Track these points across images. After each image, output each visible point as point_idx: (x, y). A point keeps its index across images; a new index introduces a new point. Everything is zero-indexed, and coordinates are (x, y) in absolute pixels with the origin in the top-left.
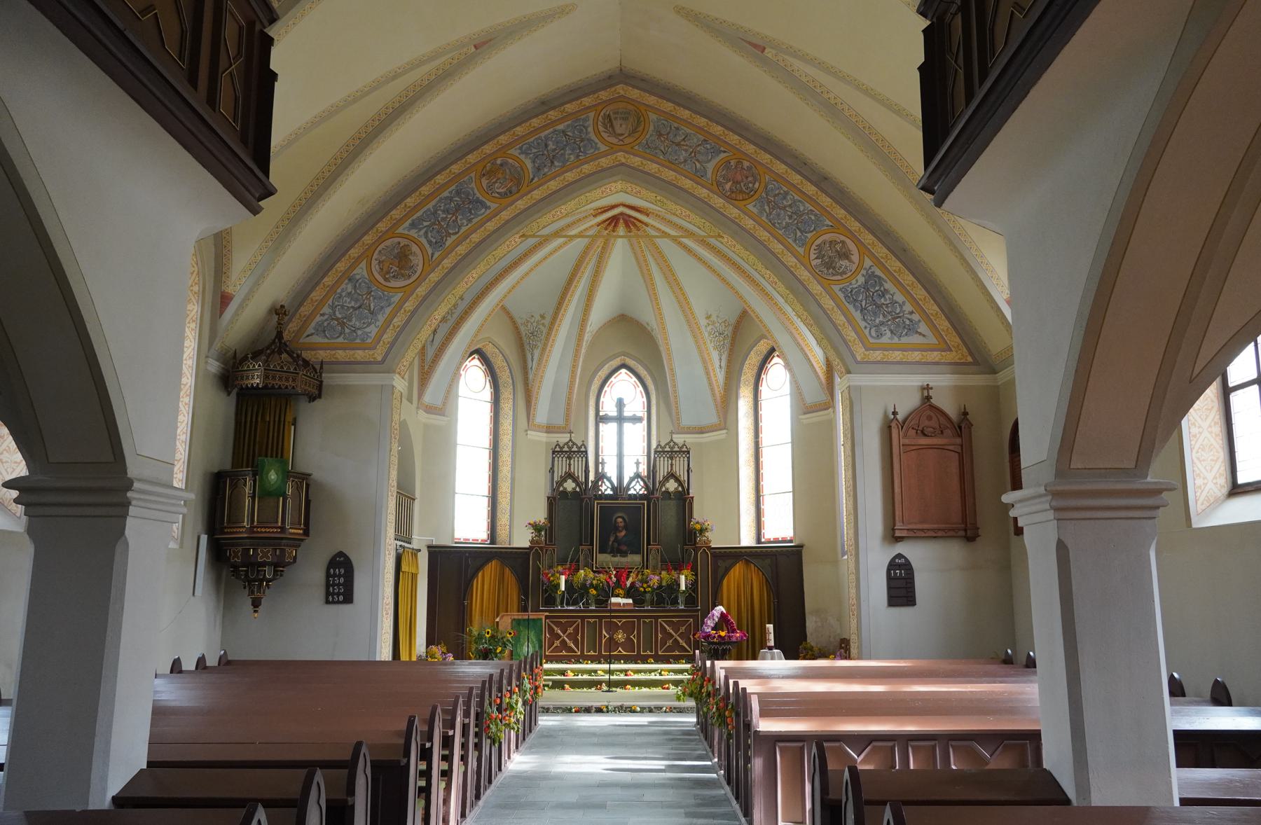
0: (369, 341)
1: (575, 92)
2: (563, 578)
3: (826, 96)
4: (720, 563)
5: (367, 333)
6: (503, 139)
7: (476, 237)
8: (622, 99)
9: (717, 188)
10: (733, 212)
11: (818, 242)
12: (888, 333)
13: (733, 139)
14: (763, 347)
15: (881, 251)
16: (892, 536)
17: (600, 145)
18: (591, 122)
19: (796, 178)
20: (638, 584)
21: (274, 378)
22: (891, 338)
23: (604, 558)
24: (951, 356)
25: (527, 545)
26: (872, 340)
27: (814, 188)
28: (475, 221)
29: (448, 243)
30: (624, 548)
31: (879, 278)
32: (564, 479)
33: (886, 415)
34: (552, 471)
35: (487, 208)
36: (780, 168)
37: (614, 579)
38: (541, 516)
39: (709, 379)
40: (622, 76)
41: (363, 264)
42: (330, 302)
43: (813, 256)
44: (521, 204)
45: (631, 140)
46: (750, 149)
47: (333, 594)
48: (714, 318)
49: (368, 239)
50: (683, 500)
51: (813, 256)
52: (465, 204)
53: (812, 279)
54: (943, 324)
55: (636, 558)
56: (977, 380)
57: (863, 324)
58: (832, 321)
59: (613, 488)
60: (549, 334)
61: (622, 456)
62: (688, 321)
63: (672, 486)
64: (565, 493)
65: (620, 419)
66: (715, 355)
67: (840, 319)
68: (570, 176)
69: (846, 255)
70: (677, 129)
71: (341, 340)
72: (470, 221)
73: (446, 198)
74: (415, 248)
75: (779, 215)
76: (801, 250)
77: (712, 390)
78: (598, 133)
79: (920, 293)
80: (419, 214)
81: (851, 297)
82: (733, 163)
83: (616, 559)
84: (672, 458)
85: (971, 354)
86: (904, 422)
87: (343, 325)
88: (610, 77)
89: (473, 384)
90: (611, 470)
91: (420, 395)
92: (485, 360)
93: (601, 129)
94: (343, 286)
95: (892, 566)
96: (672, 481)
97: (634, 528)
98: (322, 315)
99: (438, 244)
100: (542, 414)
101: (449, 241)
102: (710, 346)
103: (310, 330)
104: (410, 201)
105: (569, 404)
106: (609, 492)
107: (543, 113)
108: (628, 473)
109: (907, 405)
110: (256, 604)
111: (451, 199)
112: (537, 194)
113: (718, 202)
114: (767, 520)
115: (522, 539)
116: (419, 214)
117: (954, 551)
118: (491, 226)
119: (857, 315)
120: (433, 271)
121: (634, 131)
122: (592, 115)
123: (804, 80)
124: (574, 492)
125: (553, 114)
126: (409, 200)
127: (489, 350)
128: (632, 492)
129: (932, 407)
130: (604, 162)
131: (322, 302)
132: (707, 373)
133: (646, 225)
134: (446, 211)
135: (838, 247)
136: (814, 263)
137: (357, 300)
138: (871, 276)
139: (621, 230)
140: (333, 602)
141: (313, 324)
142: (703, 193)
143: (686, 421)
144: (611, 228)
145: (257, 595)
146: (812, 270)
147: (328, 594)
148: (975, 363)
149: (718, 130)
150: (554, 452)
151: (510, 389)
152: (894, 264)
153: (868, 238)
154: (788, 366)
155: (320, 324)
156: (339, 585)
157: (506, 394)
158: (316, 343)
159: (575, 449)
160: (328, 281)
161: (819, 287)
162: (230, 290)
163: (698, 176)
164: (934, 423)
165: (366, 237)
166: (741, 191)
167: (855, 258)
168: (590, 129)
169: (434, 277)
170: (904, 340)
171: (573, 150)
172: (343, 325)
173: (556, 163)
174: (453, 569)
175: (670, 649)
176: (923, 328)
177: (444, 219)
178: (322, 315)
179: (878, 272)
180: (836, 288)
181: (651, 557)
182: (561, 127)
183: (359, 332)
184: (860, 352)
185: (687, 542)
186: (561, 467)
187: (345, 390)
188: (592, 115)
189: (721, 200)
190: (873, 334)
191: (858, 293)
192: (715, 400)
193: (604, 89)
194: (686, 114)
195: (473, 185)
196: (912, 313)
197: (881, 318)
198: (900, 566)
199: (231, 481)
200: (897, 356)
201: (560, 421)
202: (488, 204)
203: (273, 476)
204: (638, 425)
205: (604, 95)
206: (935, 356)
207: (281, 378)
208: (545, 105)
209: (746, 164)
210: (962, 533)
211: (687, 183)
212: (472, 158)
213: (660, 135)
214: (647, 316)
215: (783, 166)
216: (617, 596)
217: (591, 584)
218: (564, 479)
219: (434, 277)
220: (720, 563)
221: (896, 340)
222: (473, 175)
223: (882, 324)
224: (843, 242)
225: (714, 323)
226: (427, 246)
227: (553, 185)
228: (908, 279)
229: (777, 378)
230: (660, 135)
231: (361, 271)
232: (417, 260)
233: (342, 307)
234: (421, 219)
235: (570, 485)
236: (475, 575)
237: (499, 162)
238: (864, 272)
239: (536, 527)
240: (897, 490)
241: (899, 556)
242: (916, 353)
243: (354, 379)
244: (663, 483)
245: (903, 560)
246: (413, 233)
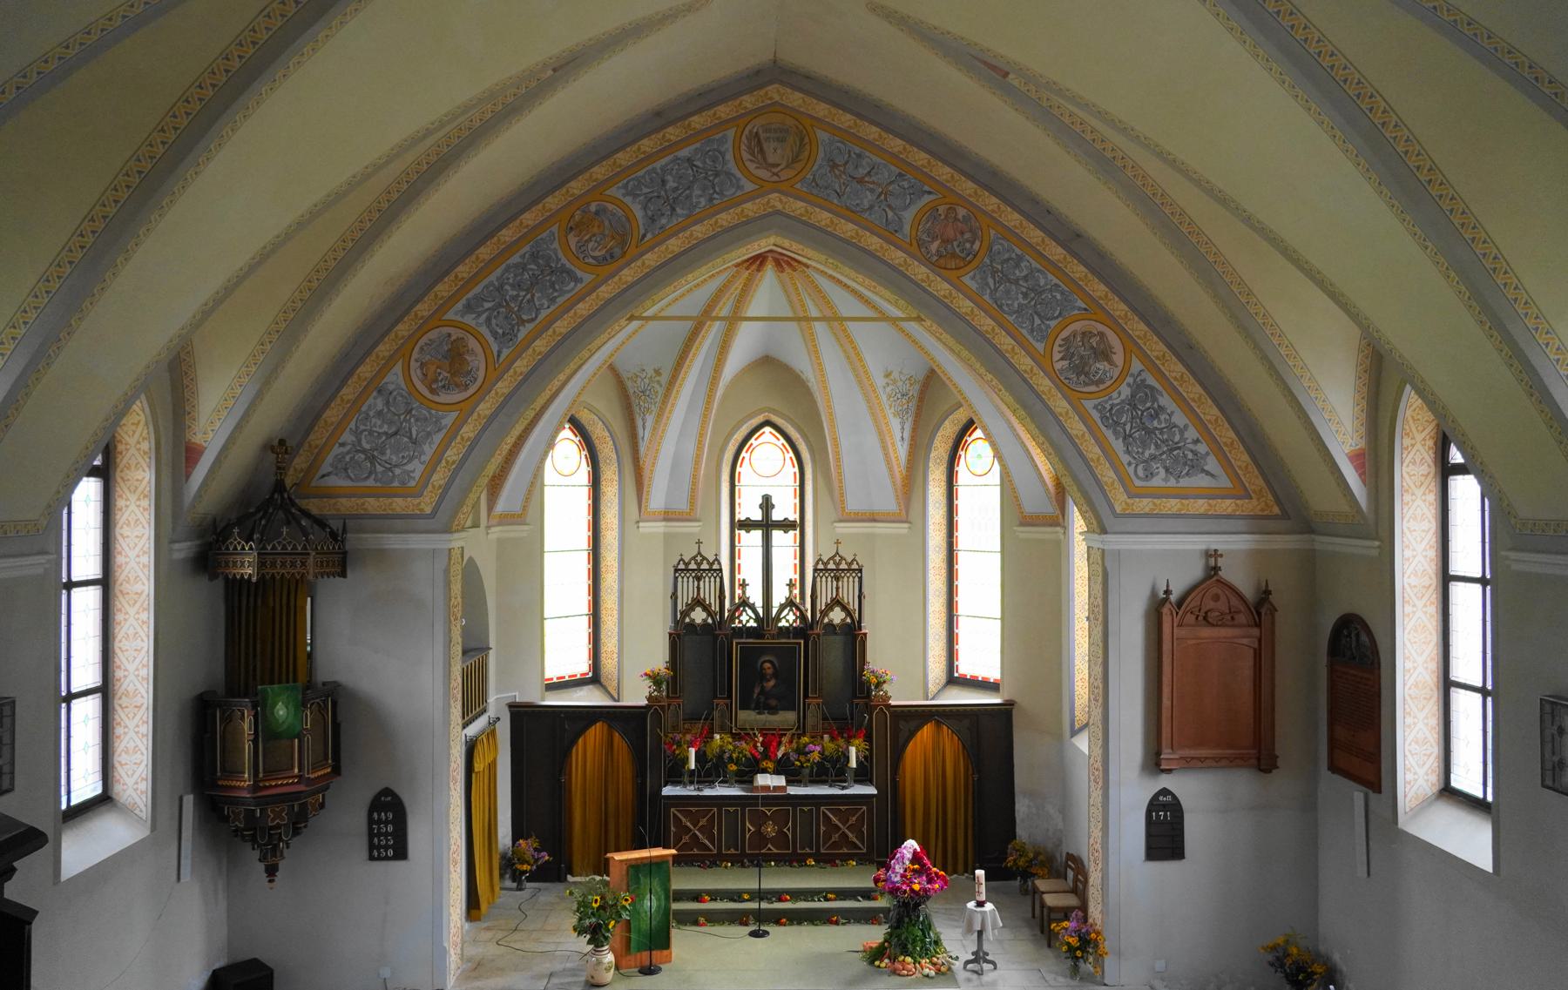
0: (413, 483)
1: (706, 98)
2: (692, 751)
3: (1098, 146)
4: (902, 724)
5: (408, 473)
6: (600, 172)
7: (562, 326)
8: (777, 108)
9: (918, 248)
10: (941, 287)
11: (1064, 334)
12: (1162, 471)
13: (943, 172)
14: (961, 416)
15: (1156, 348)
16: (1154, 763)
17: (744, 181)
18: (729, 145)
19: (1034, 235)
20: (793, 756)
21: (273, 564)
22: (1166, 480)
23: (747, 717)
24: (1249, 507)
25: (644, 702)
26: (1138, 483)
27: (1060, 250)
28: (560, 300)
29: (521, 336)
30: (773, 702)
31: (1152, 388)
32: (691, 607)
33: (1154, 593)
34: (674, 596)
35: (577, 280)
36: (1012, 218)
37: (761, 749)
38: (658, 658)
39: (886, 455)
40: (776, 72)
41: (398, 368)
42: (352, 425)
43: (1057, 356)
44: (628, 275)
45: (791, 173)
46: (967, 187)
47: (379, 847)
48: (895, 375)
49: (403, 329)
50: (853, 635)
51: (1057, 356)
52: (545, 275)
53: (1054, 390)
54: (1241, 458)
55: (789, 717)
56: (1286, 542)
57: (1125, 458)
58: (1081, 454)
59: (757, 619)
60: (667, 395)
61: (767, 578)
62: (860, 382)
63: (837, 616)
64: (692, 624)
65: (767, 525)
66: (895, 424)
67: (1093, 451)
68: (700, 231)
69: (1104, 354)
70: (859, 156)
71: (370, 482)
72: (553, 300)
73: (516, 266)
74: (472, 343)
75: (1008, 292)
76: (1040, 346)
77: (890, 469)
78: (739, 160)
79: (1210, 412)
80: (477, 290)
81: (1111, 418)
82: (942, 209)
83: (763, 717)
84: (837, 579)
85: (1278, 502)
86: (1180, 603)
87: (372, 459)
88: (758, 72)
89: (564, 464)
90: (755, 595)
91: (490, 509)
92: (578, 426)
93: (746, 156)
94: (371, 400)
95: (1154, 805)
96: (837, 609)
97: (786, 675)
98: (342, 445)
99: (507, 337)
100: (657, 498)
101: (523, 332)
102: (890, 413)
103: (326, 467)
104: (463, 270)
105: (694, 484)
106: (752, 624)
107: (657, 131)
108: (780, 595)
109: (1181, 579)
110: (271, 871)
111: (523, 267)
112: (651, 259)
113: (920, 271)
114: (962, 647)
115: (636, 694)
116: (477, 290)
117: (1242, 784)
118: (583, 309)
119: (1118, 445)
120: (499, 378)
121: (795, 160)
122: (731, 133)
123: (1067, 120)
124: (705, 624)
125: (673, 133)
126: (460, 268)
127: (585, 417)
128: (783, 623)
129: (1222, 582)
130: (750, 208)
131: (340, 426)
132: (884, 448)
133: (807, 266)
134: (518, 286)
135: (1094, 341)
136: (1058, 366)
137: (391, 423)
138: (1140, 386)
139: (769, 270)
140: (379, 859)
141: (330, 459)
142: (897, 257)
143: (853, 505)
144: (754, 267)
145: (271, 861)
146: (1054, 376)
147: (371, 847)
148: (1285, 515)
149: (920, 158)
150: (676, 570)
151: (614, 467)
152: (1175, 369)
153: (1138, 328)
154: (989, 437)
155: (340, 458)
156: (386, 834)
157: (609, 475)
158: (338, 488)
159: (705, 566)
160: (348, 392)
161: (1064, 403)
162: (198, 439)
163: (890, 232)
164: (1222, 605)
165: (400, 326)
166: (954, 255)
167: (1118, 358)
168: (729, 156)
169: (503, 387)
170: (1184, 482)
171: (704, 189)
172: (373, 460)
173: (678, 210)
174: (542, 734)
175: (835, 845)
176: (1212, 464)
177: (514, 298)
178: (342, 445)
179: (1151, 381)
180: (1089, 405)
181: (809, 714)
182: (685, 153)
183: (397, 471)
184: (1120, 499)
185: (854, 701)
186: (687, 591)
187: (381, 555)
188: (731, 133)
189: (923, 269)
190: (1141, 472)
191: (1120, 412)
192: (894, 483)
193: (750, 91)
194: (871, 132)
195: (556, 245)
196: (1196, 442)
197: (1152, 450)
198: (1164, 806)
199: (222, 714)
200: (1173, 505)
201: (683, 505)
202: (579, 274)
203: (281, 711)
204: (791, 533)
205: (748, 101)
206: (1227, 506)
207: (283, 564)
208: (659, 118)
209: (961, 212)
210: (1254, 761)
211: (873, 242)
212: (553, 202)
213: (834, 166)
214: (801, 363)
215: (1016, 216)
216: (764, 771)
217: (731, 758)
218: (691, 607)
219: (503, 387)
220: (902, 724)
221: (1172, 482)
222: (555, 229)
223: (1153, 458)
224: (1101, 334)
225: (895, 382)
226: (491, 339)
227: (674, 245)
228: (1193, 390)
229: (978, 456)
230: (834, 166)
231: (395, 377)
232: (477, 362)
233: (371, 432)
234: (480, 299)
235: (699, 616)
236: (574, 742)
237: (593, 208)
238: (1130, 380)
239: (655, 679)
240: (1166, 702)
241: (1165, 792)
242: (1201, 502)
243: (394, 542)
244: (824, 613)
245: (1169, 798)
246: (469, 319)
